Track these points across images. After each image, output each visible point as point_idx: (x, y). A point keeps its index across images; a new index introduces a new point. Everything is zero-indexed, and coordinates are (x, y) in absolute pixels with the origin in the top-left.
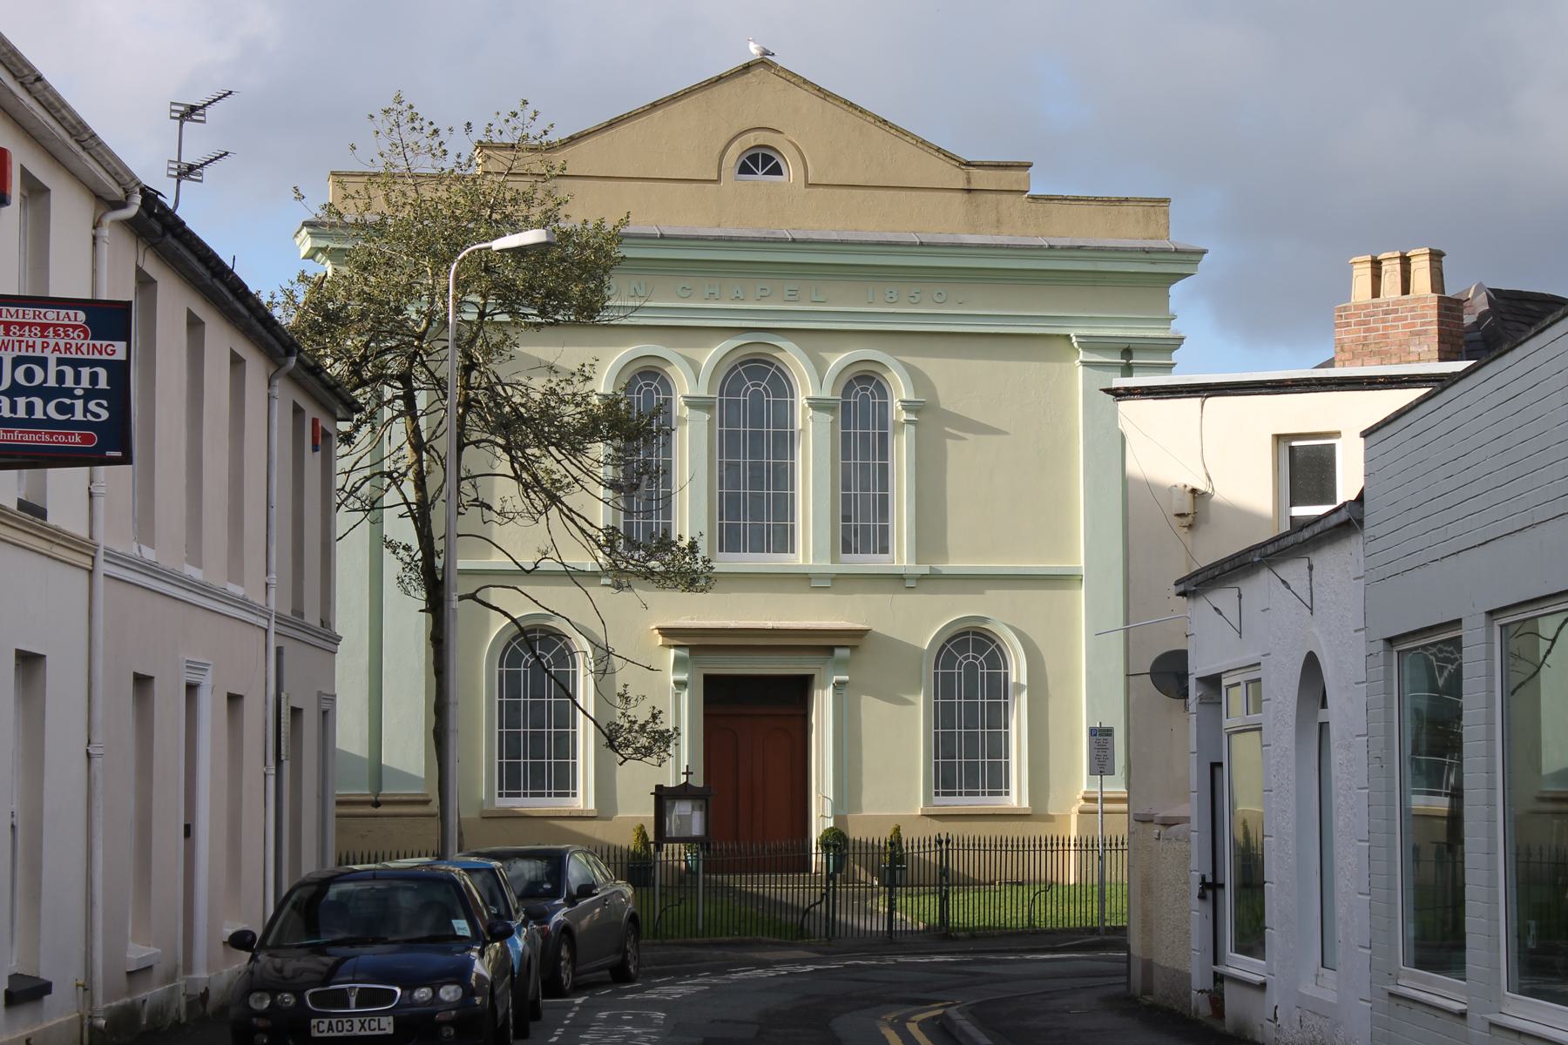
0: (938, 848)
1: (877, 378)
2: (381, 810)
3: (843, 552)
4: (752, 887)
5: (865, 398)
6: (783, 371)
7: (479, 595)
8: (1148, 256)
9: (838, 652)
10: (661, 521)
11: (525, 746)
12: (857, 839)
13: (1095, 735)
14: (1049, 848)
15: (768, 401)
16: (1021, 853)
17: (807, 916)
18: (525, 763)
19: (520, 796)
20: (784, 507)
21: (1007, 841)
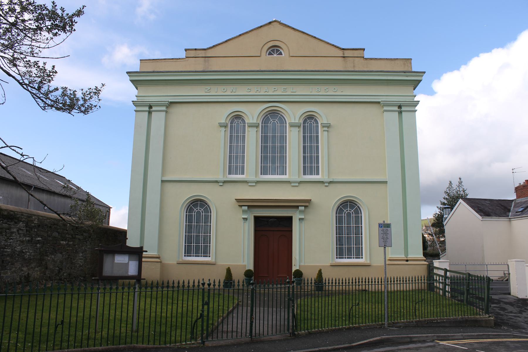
1: (242, 117)
2: (408, 263)
3: (303, 175)
4: (285, 291)
5: (311, 124)
6: (283, 116)
8: (405, 74)
9: (300, 208)
11: (194, 240)
12: (482, 276)
13: (382, 227)
15: (314, 126)
18: (193, 245)
19: (191, 256)
20: (283, 159)
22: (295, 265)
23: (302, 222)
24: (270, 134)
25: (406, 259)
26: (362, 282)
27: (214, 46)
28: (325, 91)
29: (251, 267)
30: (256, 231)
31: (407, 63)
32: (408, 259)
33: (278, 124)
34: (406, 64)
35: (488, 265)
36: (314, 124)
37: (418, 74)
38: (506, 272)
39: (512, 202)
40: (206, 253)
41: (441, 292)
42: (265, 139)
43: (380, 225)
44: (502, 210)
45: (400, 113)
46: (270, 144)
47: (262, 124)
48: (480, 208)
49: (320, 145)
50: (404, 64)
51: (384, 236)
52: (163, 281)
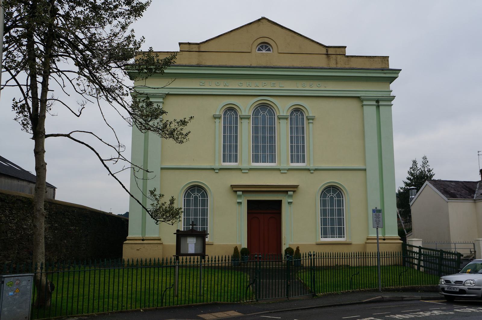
0: (310, 258)
3: (291, 163)
5: (297, 116)
7: (71, 135)
9: (289, 193)
10: (337, 227)
13: (375, 212)
14: (358, 257)
16: (344, 259)
17: (249, 288)
20: (272, 149)
21: (345, 254)
22: (285, 244)
23: (290, 205)
24: (260, 125)
25: (383, 238)
26: (361, 255)
27: (207, 41)
28: (311, 86)
29: (245, 245)
30: (248, 213)
31: (385, 60)
32: (385, 238)
33: (267, 116)
34: (384, 61)
35: (456, 244)
36: (300, 116)
37: (394, 72)
38: (472, 250)
39: (477, 184)
40: (341, 233)
41: (416, 267)
42: (256, 130)
43: (373, 210)
44: (468, 192)
45: (378, 106)
46: (260, 134)
47: (253, 116)
48: (446, 190)
49: (305, 135)
50: (382, 62)
51: (377, 219)
52: (155, 259)
